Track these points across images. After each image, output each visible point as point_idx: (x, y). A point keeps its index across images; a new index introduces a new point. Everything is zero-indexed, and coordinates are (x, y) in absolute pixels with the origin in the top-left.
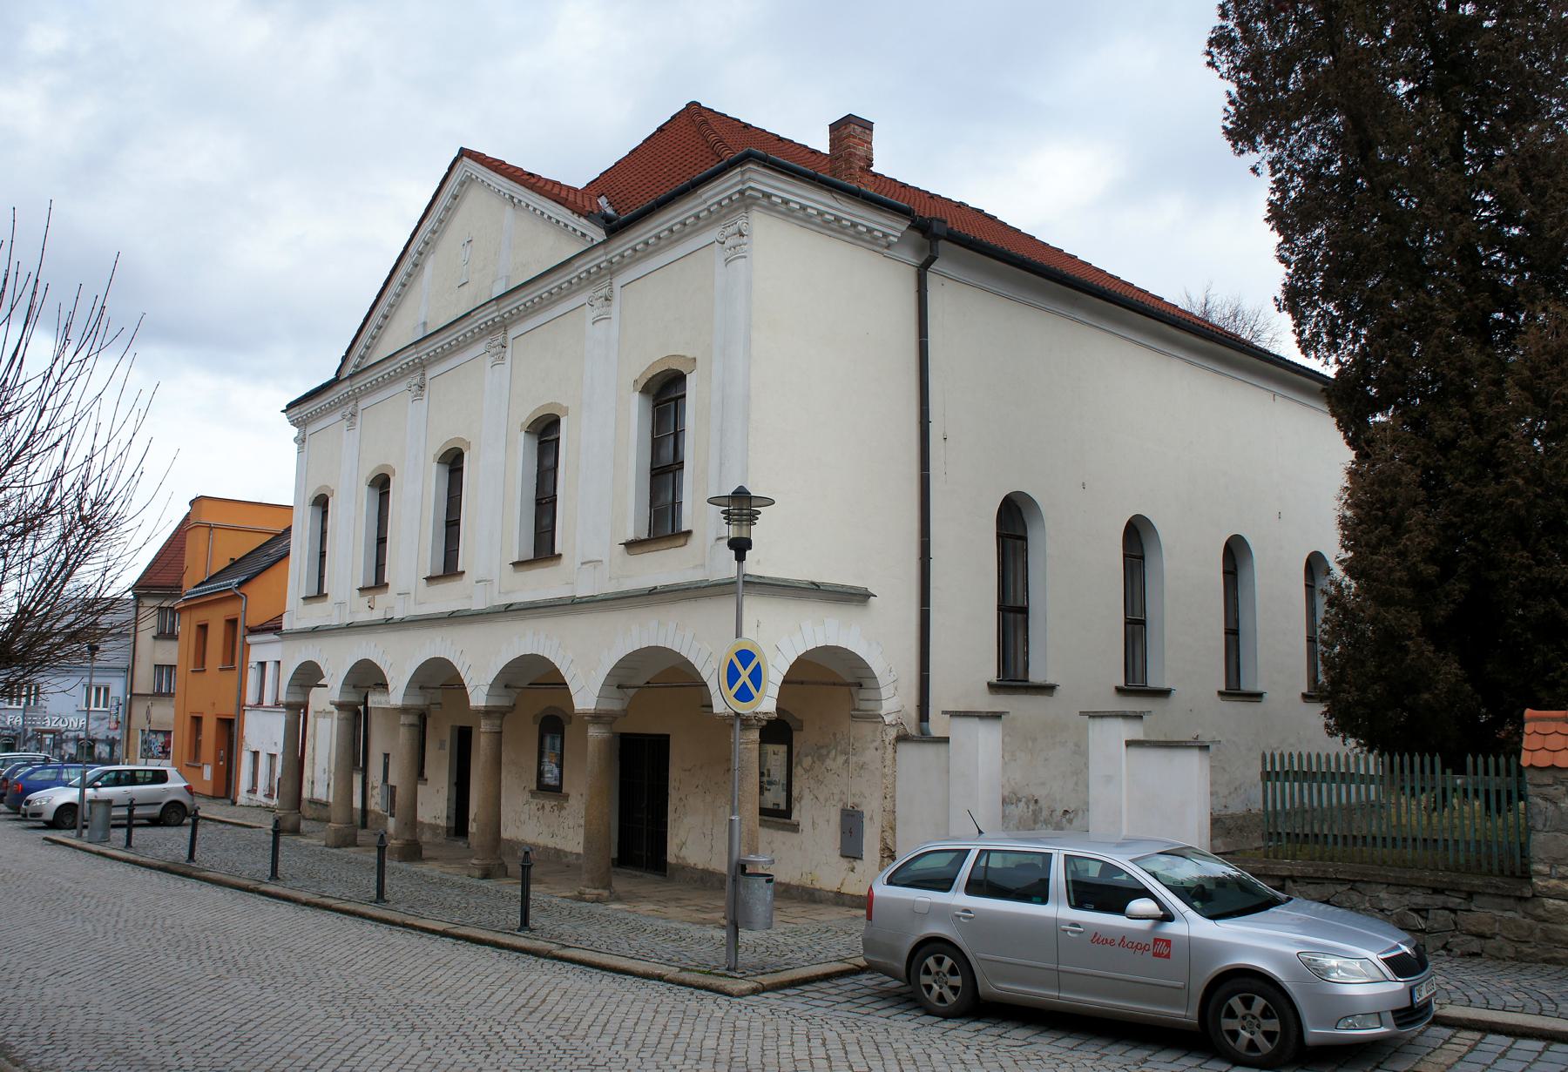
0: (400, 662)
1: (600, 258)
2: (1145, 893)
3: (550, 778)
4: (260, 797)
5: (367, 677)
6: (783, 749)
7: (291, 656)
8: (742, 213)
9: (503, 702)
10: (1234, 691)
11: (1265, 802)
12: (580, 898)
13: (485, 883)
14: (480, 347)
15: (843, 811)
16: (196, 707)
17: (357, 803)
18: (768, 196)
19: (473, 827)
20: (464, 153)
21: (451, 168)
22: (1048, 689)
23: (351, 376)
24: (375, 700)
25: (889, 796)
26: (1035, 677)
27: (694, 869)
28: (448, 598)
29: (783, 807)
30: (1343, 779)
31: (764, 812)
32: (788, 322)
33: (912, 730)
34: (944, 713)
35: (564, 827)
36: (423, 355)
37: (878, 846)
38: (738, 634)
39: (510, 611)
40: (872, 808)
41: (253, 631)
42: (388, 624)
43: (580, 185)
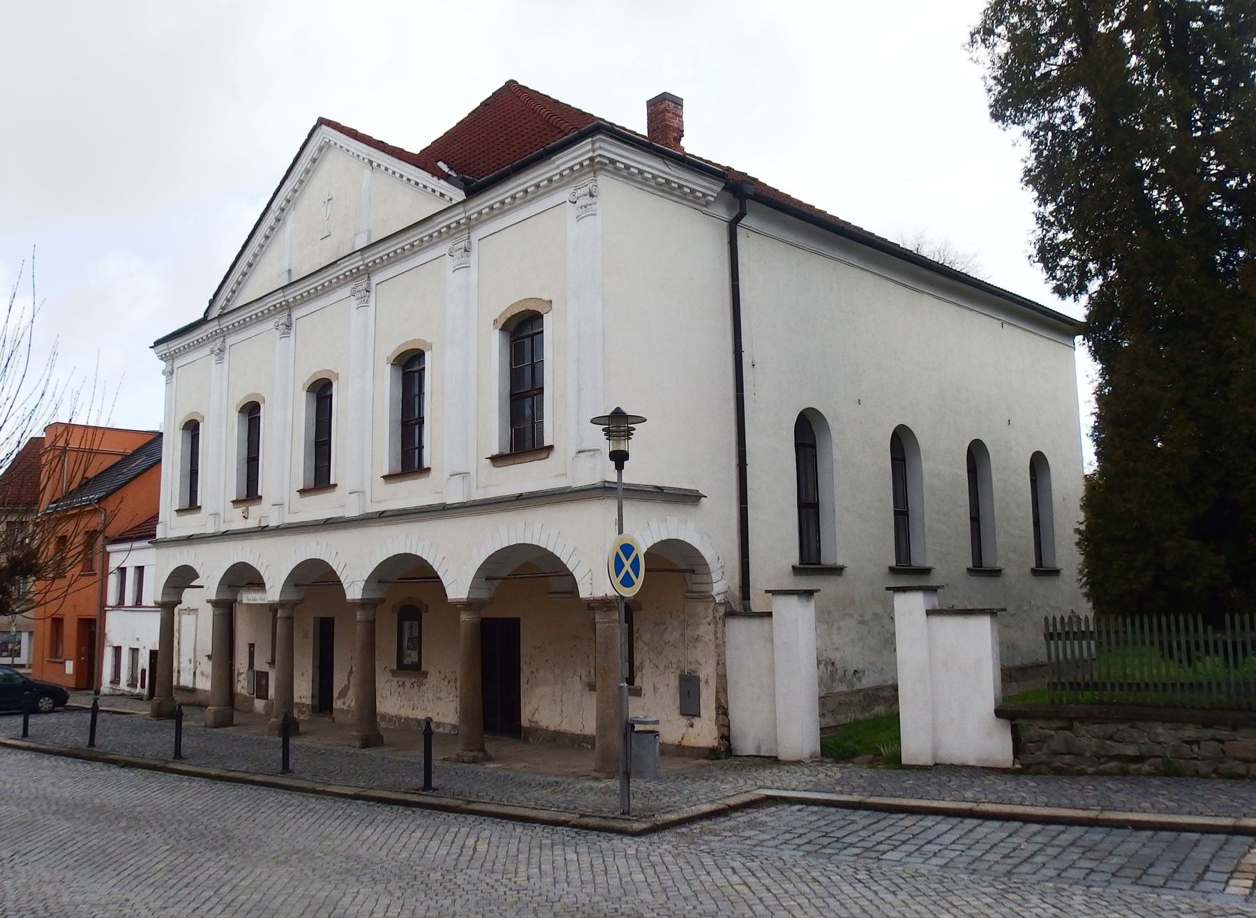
0: (276, 564)
1: (459, 215)
9: (376, 595)
11: (1049, 657)
12: (460, 760)
13: (366, 751)
14: (346, 291)
18: (613, 162)
21: (310, 135)
23: (220, 316)
24: (249, 597)
25: (721, 663)
27: (546, 730)
35: (439, 702)
38: (620, 532)
39: (383, 517)
40: (707, 672)
42: (263, 531)
43: (417, 151)
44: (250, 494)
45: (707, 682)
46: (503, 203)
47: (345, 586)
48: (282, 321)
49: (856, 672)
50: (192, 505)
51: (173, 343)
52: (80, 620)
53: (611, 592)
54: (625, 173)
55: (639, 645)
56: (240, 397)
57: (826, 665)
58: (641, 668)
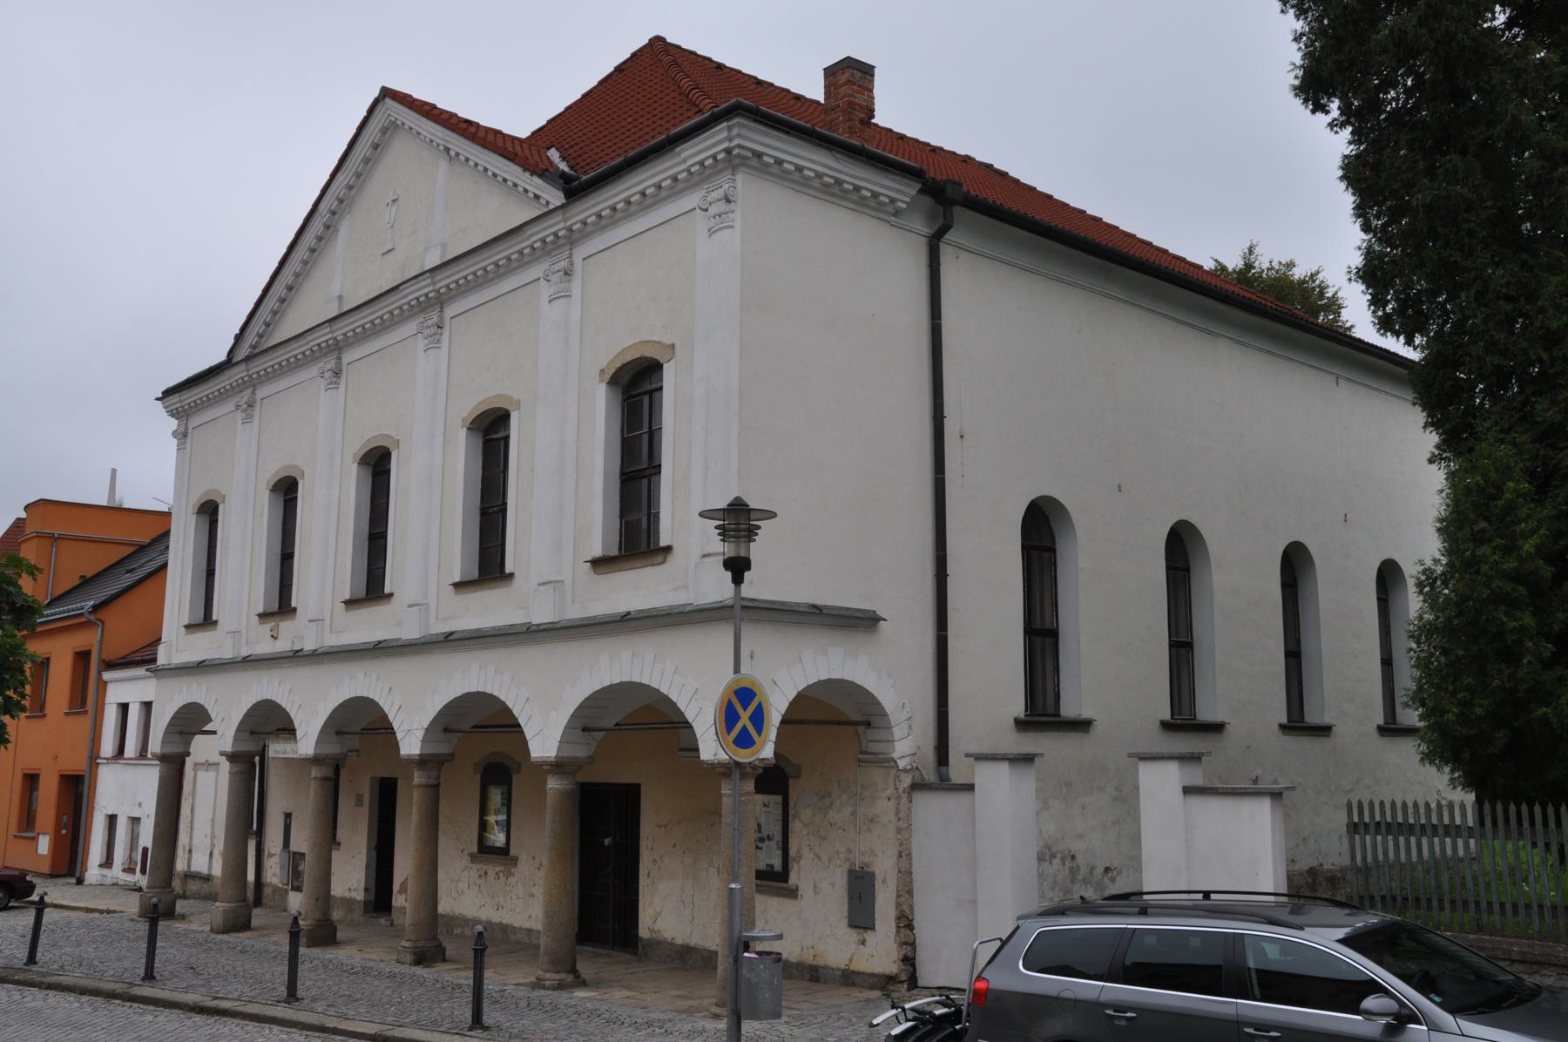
0: (311, 705)
1: (557, 225)
2: (1373, 987)
3: (498, 838)
4: (117, 872)
5: (268, 722)
6: (779, 798)
7: (169, 699)
8: (727, 175)
9: (442, 749)
10: (1297, 724)
11: (1353, 858)
12: (538, 984)
13: (419, 971)
14: (410, 328)
15: (851, 872)
16: (29, 763)
17: (251, 877)
18: (759, 155)
19: (398, 900)
20: (386, 93)
21: (371, 111)
22: (1083, 725)
23: (248, 359)
25: (904, 855)
26: (1069, 709)
28: (371, 625)
29: (778, 866)
30: (1447, 834)
31: (760, 875)
32: (704, 262)
33: (930, 776)
34: (967, 755)
35: (522, 896)
36: (339, 335)
37: (892, 914)
39: (451, 641)
40: (884, 867)
41: (111, 665)
42: (296, 657)
43: (523, 132)
44: (282, 606)
45: (884, 881)
46: (614, 209)
47: (399, 736)
48: (329, 366)
49: (1107, 869)
50: (206, 621)
51: (188, 396)
52: (63, 777)
53: (723, 757)
54: (776, 169)
55: (795, 825)
56: (273, 470)
57: (1063, 860)
58: (799, 857)
